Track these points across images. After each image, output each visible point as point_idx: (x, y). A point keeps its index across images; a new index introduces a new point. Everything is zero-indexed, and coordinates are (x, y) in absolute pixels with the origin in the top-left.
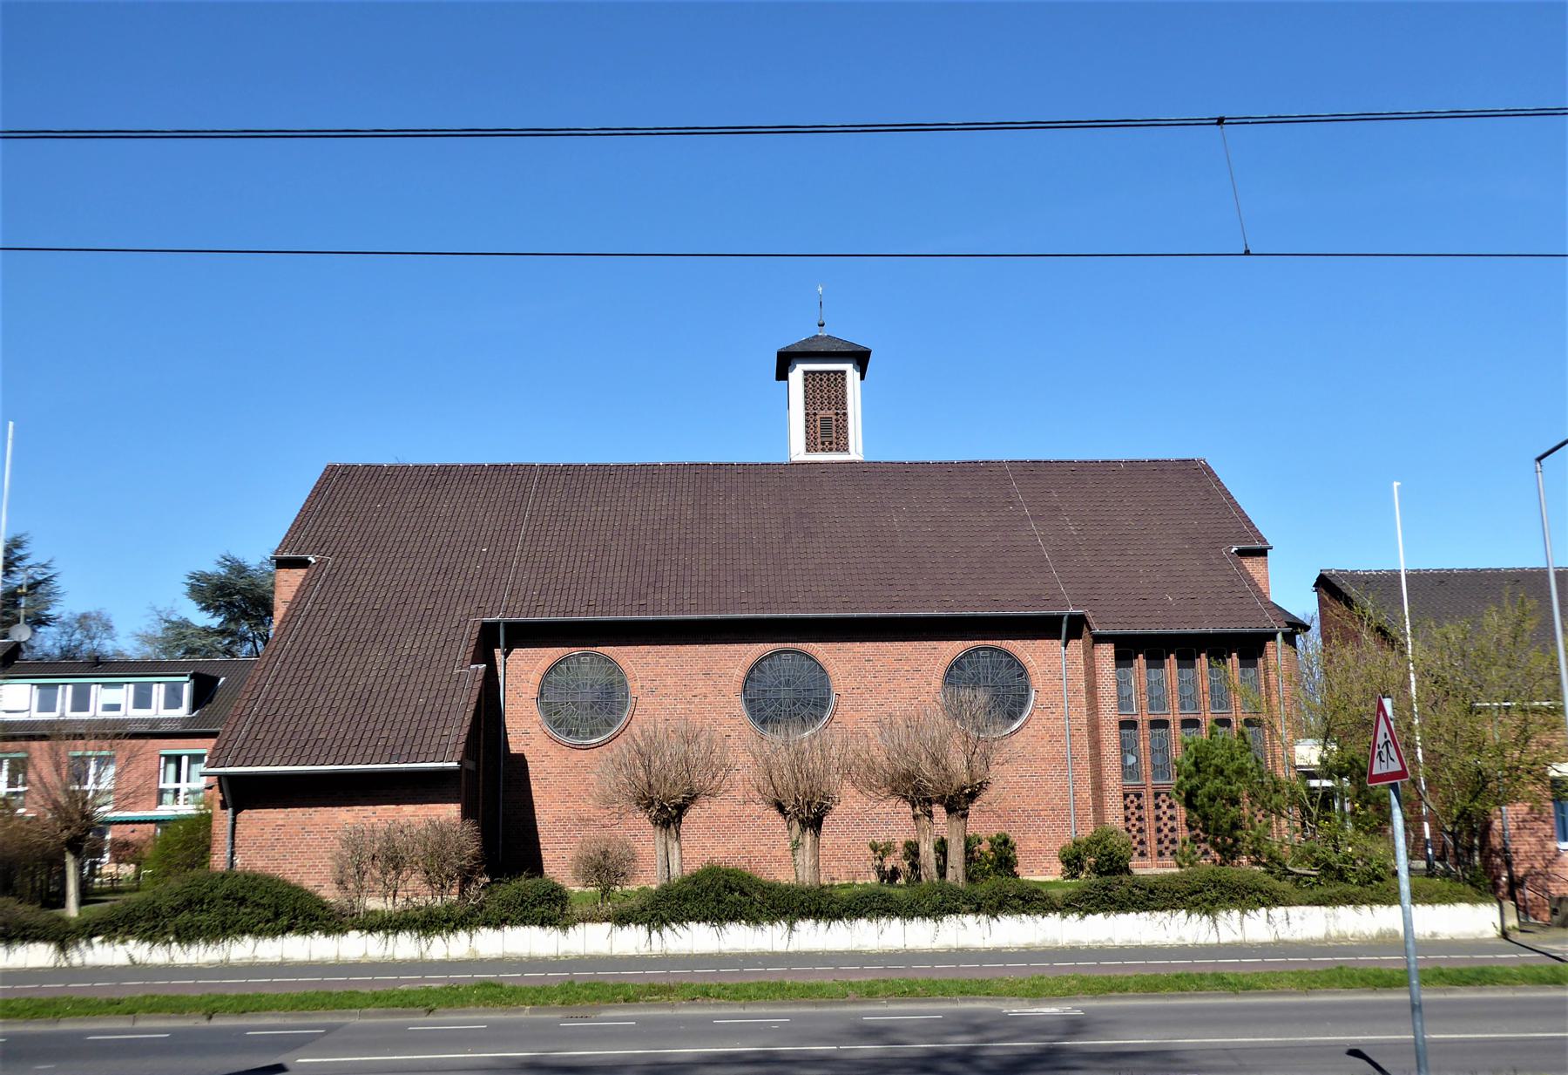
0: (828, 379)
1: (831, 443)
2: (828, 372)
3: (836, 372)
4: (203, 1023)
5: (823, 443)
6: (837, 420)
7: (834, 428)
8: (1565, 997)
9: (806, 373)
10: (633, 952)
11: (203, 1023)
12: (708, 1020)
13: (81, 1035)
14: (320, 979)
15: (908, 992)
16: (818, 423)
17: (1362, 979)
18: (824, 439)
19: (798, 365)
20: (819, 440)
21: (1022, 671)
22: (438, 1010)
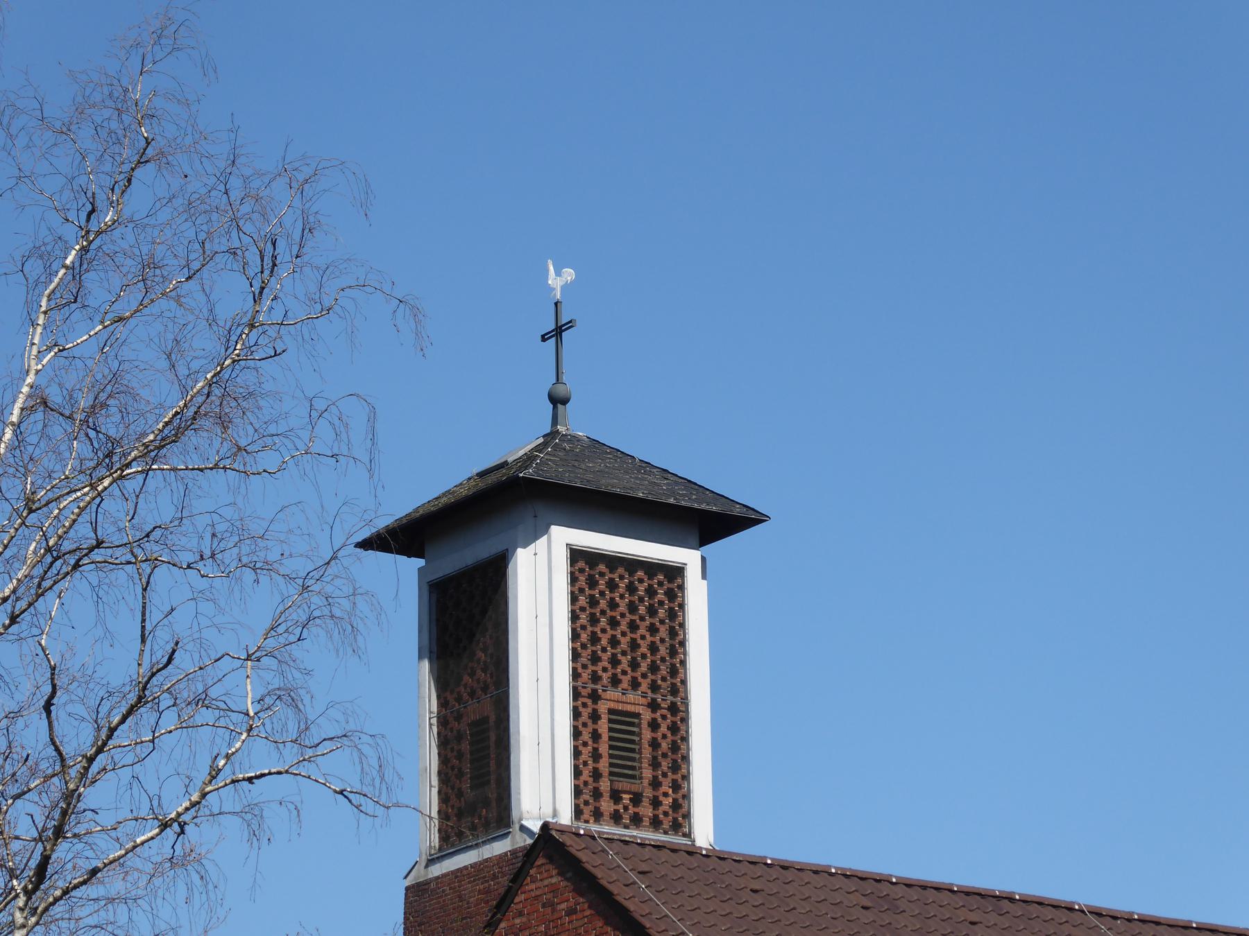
1: (637, 799)
9: (576, 555)
16: (603, 726)
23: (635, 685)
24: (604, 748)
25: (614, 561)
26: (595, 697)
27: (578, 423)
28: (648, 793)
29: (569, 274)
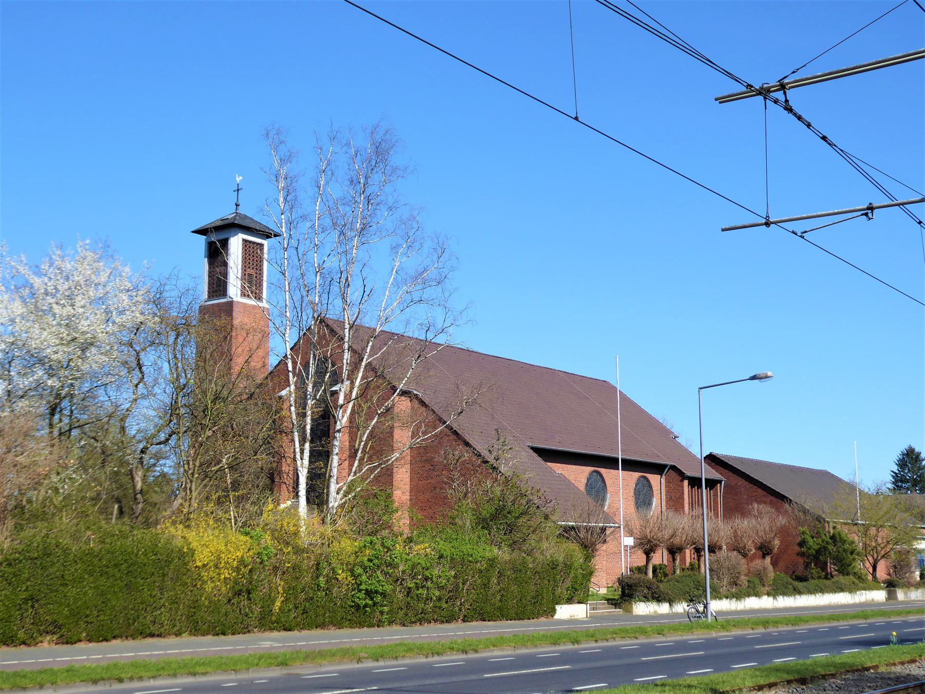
0: (253, 248)
2: (254, 243)
3: (258, 244)
6: (256, 277)
9: (244, 240)
19: (239, 234)
21: (650, 486)
23: (253, 268)
25: (250, 242)
27: (241, 210)
29: (241, 178)
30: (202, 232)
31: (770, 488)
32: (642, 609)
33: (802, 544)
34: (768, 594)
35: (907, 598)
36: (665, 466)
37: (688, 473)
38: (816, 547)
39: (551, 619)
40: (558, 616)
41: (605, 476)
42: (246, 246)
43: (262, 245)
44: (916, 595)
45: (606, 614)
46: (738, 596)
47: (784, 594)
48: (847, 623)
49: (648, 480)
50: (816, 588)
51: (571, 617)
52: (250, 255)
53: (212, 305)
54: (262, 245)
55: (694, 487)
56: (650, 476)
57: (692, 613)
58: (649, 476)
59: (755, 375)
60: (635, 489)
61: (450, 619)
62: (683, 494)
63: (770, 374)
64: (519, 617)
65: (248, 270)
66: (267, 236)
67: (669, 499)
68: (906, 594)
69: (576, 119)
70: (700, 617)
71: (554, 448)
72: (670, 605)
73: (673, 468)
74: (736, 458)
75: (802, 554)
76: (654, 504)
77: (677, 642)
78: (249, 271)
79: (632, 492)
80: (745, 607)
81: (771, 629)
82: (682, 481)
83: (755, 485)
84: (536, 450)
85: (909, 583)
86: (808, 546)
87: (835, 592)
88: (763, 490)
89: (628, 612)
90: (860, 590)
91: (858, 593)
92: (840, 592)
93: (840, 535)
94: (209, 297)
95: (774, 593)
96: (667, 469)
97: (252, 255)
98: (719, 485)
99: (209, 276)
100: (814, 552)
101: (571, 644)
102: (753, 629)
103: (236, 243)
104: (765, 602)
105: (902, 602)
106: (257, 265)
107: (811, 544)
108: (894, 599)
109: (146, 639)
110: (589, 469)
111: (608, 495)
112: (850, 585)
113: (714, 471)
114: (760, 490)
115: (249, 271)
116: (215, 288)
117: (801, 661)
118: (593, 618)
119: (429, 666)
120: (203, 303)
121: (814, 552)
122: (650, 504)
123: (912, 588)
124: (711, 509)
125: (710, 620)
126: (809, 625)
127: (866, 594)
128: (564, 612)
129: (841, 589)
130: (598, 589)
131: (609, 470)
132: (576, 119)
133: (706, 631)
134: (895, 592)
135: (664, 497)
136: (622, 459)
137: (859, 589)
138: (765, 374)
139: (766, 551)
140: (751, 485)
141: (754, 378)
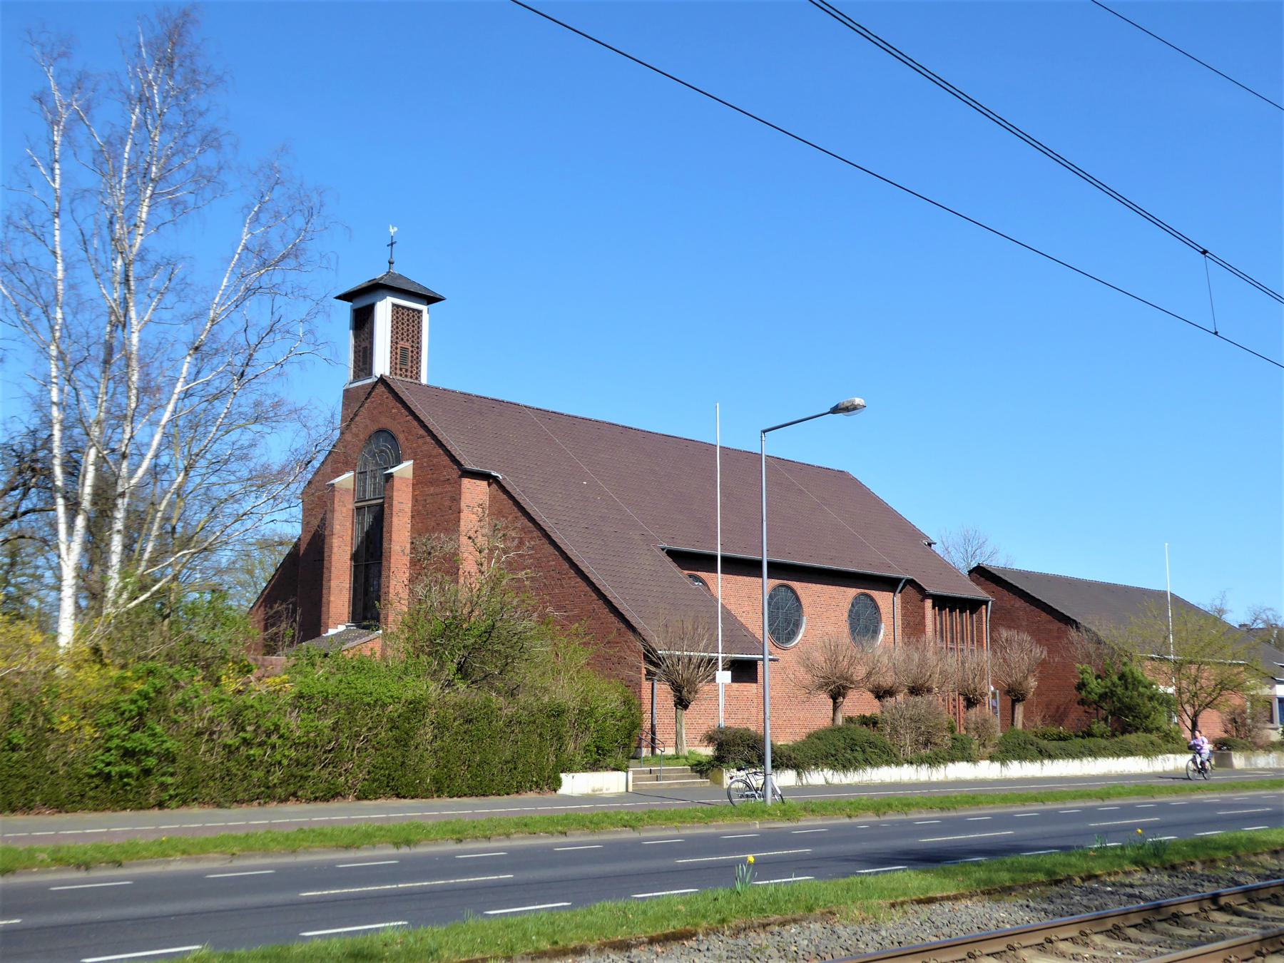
0: (408, 315)
1: (406, 371)
2: (409, 309)
3: (414, 310)
4: (847, 820)
5: (401, 370)
6: (412, 352)
7: (410, 359)
8: (1282, 794)
9: (394, 305)
10: (996, 778)
11: (847, 820)
12: (962, 819)
13: (1056, 811)
14: (105, 830)
15: (1024, 799)
16: (399, 351)
17: (805, 809)
18: (403, 366)
19: (388, 298)
20: (398, 366)
21: (876, 607)
22: (362, 847)
23: (408, 340)
24: (398, 357)
25: (404, 308)
26: (397, 343)
27: (396, 270)
28: (410, 369)
29: (396, 229)
30: (347, 297)
31: (1057, 610)
32: (1238, 761)
33: (1082, 686)
34: (992, 758)
35: (1251, 764)
36: (898, 580)
37: (931, 590)
38: (1100, 690)
39: (550, 796)
40: (563, 790)
41: (799, 592)
42: (398, 313)
43: (420, 312)
44: (1265, 761)
45: (676, 786)
46: (933, 761)
47: (1021, 758)
48: (1218, 796)
49: (872, 599)
50: (1083, 749)
51: (593, 791)
52: (403, 324)
53: (357, 387)
54: (420, 312)
55: (945, 609)
56: (876, 594)
57: (738, 790)
58: (875, 594)
59: (837, 406)
60: (851, 611)
61: (332, 794)
62: (924, 617)
63: (858, 401)
64: (473, 792)
65: (402, 342)
66: (431, 299)
67: (906, 626)
68: (1248, 759)
69: (1216, 333)
70: (753, 796)
71: (826, 566)
72: (799, 774)
73: (911, 582)
74: (998, 569)
75: (1082, 702)
76: (882, 631)
77: (1122, 806)
78: (401, 344)
79: (846, 615)
80: (946, 776)
81: (914, 815)
82: (922, 600)
83: (1037, 607)
84: (674, 554)
85: (1255, 743)
86: (1089, 689)
87: (1119, 756)
88: (1047, 614)
89: (717, 784)
90: (1165, 753)
91: (1160, 757)
92: (1127, 756)
93: (1132, 673)
94: (354, 377)
95: (1005, 753)
96: (901, 585)
97: (406, 326)
98: (984, 607)
99: (355, 352)
100: (1096, 697)
101: (391, 846)
102: (850, 817)
103: (384, 309)
104: (987, 770)
105: (1241, 772)
106: (413, 337)
107: (1093, 686)
108: (1227, 767)
109: (181, 808)
110: (852, 592)
111: (805, 620)
112: (1146, 746)
113: (978, 588)
114: (1044, 614)
115: (401, 344)
116: (362, 367)
117: (1232, 835)
118: (639, 793)
119: (549, 850)
120: (348, 386)
121: (1096, 697)
122: (876, 632)
123: (1260, 752)
124: (972, 641)
125: (769, 802)
126: (980, 809)
127: (1175, 759)
128: (575, 784)
129: (1130, 752)
130: (663, 749)
131: (806, 584)
132: (1216, 333)
133: (742, 820)
134: (1229, 757)
135: (899, 622)
136: (722, 557)
137: (1161, 752)
138: (849, 402)
139: (1016, 696)
140: (1033, 607)
141: (836, 410)
